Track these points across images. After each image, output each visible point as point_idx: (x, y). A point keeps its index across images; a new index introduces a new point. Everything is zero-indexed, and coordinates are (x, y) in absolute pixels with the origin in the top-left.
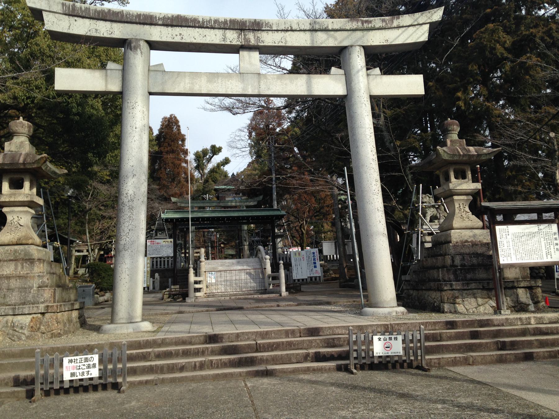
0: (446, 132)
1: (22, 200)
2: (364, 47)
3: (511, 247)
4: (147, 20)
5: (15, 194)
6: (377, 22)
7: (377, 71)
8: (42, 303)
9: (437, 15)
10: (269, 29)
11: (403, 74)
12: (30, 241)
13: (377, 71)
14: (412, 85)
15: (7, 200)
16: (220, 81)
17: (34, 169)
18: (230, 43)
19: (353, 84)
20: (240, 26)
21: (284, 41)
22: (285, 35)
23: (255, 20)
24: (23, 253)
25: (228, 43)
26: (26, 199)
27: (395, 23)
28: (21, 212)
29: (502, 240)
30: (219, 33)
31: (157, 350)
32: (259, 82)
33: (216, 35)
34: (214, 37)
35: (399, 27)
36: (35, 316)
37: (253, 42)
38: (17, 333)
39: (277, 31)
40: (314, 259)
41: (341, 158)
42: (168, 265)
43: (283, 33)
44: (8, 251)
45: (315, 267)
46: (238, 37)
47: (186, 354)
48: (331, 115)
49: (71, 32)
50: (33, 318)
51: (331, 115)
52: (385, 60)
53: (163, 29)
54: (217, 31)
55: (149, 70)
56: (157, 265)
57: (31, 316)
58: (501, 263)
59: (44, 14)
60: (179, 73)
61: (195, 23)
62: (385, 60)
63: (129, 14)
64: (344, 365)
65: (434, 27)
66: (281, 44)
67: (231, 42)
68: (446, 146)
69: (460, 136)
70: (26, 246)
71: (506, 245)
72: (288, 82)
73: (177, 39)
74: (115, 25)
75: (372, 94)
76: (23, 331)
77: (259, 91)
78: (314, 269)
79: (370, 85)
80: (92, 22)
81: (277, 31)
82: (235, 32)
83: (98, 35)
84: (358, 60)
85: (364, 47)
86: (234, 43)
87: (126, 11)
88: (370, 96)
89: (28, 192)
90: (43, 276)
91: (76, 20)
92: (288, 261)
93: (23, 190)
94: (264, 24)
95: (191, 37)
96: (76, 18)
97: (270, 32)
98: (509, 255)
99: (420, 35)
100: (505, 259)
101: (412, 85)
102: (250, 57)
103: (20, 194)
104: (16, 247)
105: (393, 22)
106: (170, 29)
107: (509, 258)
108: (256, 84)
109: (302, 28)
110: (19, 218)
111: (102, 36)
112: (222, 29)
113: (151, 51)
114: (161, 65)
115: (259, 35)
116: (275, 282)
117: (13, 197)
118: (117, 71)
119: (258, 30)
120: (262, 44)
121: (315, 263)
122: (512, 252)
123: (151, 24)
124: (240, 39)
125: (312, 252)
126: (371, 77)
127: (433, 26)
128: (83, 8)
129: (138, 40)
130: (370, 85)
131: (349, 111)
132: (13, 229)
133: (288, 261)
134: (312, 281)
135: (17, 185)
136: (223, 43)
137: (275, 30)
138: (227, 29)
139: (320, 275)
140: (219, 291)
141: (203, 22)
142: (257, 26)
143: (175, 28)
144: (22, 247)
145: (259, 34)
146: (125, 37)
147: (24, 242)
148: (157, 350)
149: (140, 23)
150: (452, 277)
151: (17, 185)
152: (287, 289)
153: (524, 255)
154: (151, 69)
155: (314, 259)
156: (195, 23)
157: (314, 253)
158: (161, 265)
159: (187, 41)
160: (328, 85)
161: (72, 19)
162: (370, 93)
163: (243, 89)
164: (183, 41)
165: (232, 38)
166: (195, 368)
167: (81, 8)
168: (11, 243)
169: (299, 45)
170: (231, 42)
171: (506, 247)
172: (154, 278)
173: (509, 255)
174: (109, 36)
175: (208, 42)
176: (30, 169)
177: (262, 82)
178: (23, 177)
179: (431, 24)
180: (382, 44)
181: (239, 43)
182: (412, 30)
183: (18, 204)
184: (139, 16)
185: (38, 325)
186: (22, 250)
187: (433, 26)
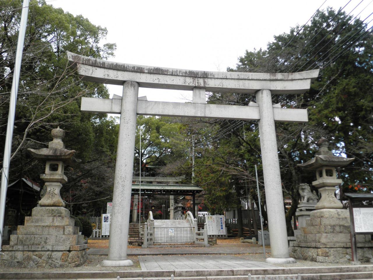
1: (58, 178)
3: (362, 222)
4: (139, 70)
5: (53, 174)
10: (212, 77)
12: (61, 204)
14: (300, 115)
15: (49, 178)
16: (181, 107)
17: (66, 159)
18: (188, 85)
20: (193, 75)
21: (221, 85)
22: (222, 81)
23: (204, 72)
24: (57, 212)
25: (187, 84)
26: (59, 178)
27: (290, 78)
29: (357, 217)
30: (182, 79)
33: (180, 80)
34: (179, 81)
35: (292, 80)
36: (65, 252)
38: (54, 262)
39: (217, 78)
40: (222, 223)
43: (221, 80)
44: (48, 210)
45: (222, 228)
46: (193, 82)
49: (93, 76)
50: (64, 253)
53: (148, 75)
55: (137, 100)
57: (62, 253)
60: (156, 102)
61: (167, 72)
63: (128, 66)
64: (274, 277)
65: (313, 81)
66: (219, 86)
67: (189, 84)
70: (59, 207)
71: (359, 220)
72: (223, 109)
73: (156, 82)
76: (57, 261)
77: (205, 114)
78: (221, 230)
80: (106, 70)
81: (217, 78)
82: (191, 78)
83: (109, 78)
85: (271, 91)
86: (191, 85)
87: (126, 64)
88: (275, 121)
89: (59, 174)
91: (96, 69)
92: (202, 222)
93: (58, 171)
94: (210, 74)
95: (164, 81)
96: (97, 68)
97: (213, 79)
98: (361, 227)
99: (306, 85)
100: (358, 229)
101: (300, 115)
102: (200, 94)
103: (56, 174)
104: (53, 208)
105: (288, 77)
106: (152, 75)
107: (361, 229)
110: (54, 189)
111: (111, 78)
112: (184, 76)
113: (140, 88)
114: (145, 97)
117: (52, 176)
118: (119, 100)
119: (206, 78)
120: (208, 86)
121: (222, 226)
122: (362, 225)
124: (194, 83)
125: (220, 218)
127: (313, 81)
128: (101, 62)
131: (261, 129)
132: (51, 196)
133: (202, 222)
134: (220, 237)
135: (54, 168)
136: (184, 84)
137: (216, 78)
138: (187, 76)
139: (225, 234)
140: (163, 241)
141: (172, 72)
142: (205, 76)
143: (155, 75)
144: (56, 208)
145: (206, 80)
147: (57, 204)
151: (54, 168)
153: (369, 227)
154: (139, 99)
155: (222, 223)
156: (167, 72)
157: (221, 219)
159: (162, 83)
161: (94, 68)
162: (274, 118)
164: (160, 83)
165: (189, 81)
168: (50, 205)
169: (231, 87)
170: (189, 84)
171: (359, 222)
173: (361, 227)
174: (115, 79)
175: (175, 84)
176: (63, 159)
177: (207, 109)
178: (58, 163)
179: (312, 79)
180: (282, 89)
181: (194, 85)
183: (55, 180)
184: (134, 67)
185: (67, 258)
186: (56, 210)
187: (313, 81)
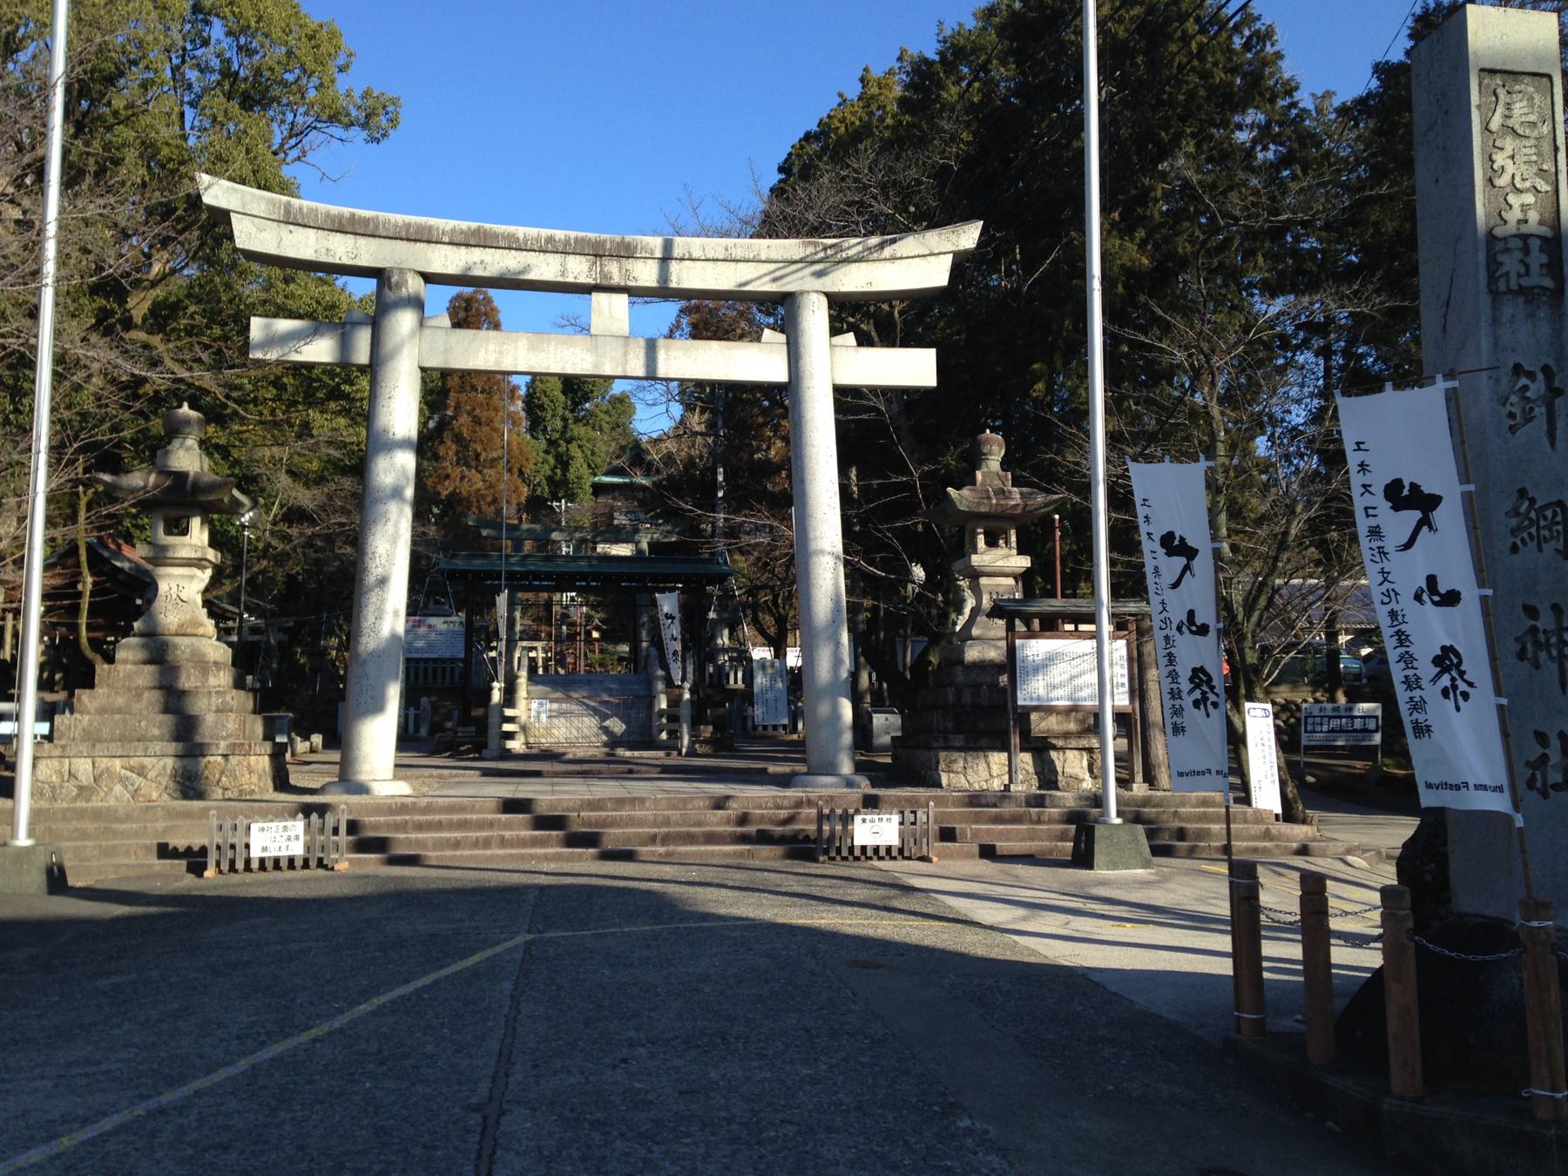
0: (975, 459)
2: (827, 295)
6: (853, 245)
7: (850, 338)
8: (225, 738)
9: (968, 236)
11: (893, 345)
13: (850, 338)
14: (914, 367)
16: (552, 348)
19: (802, 362)
26: (193, 555)
28: (183, 576)
31: (417, 818)
32: (626, 354)
35: (894, 258)
37: (617, 279)
41: (779, 492)
42: (452, 678)
47: (463, 825)
48: (774, 405)
51: (774, 405)
52: (863, 318)
54: (550, 257)
56: (426, 678)
58: (1020, 703)
59: (234, 218)
62: (863, 318)
65: (962, 264)
68: (974, 483)
69: (1006, 464)
70: (194, 639)
74: (362, 241)
75: (839, 382)
79: (836, 364)
82: (583, 258)
84: (815, 317)
85: (827, 295)
90: (224, 693)
99: (936, 274)
101: (914, 367)
108: (619, 353)
109: (710, 256)
115: (629, 267)
116: (673, 726)
123: (429, 242)
126: (837, 351)
129: (402, 271)
130: (836, 364)
136: (561, 279)
146: (380, 266)
147: (189, 631)
148: (417, 818)
149: (409, 240)
150: (950, 725)
152: (1119, 814)
158: (435, 678)
160: (754, 361)
161: (285, 228)
163: (596, 366)
166: (476, 844)
167: (301, 209)
172: (417, 708)
181: (591, 281)
182: (921, 263)
